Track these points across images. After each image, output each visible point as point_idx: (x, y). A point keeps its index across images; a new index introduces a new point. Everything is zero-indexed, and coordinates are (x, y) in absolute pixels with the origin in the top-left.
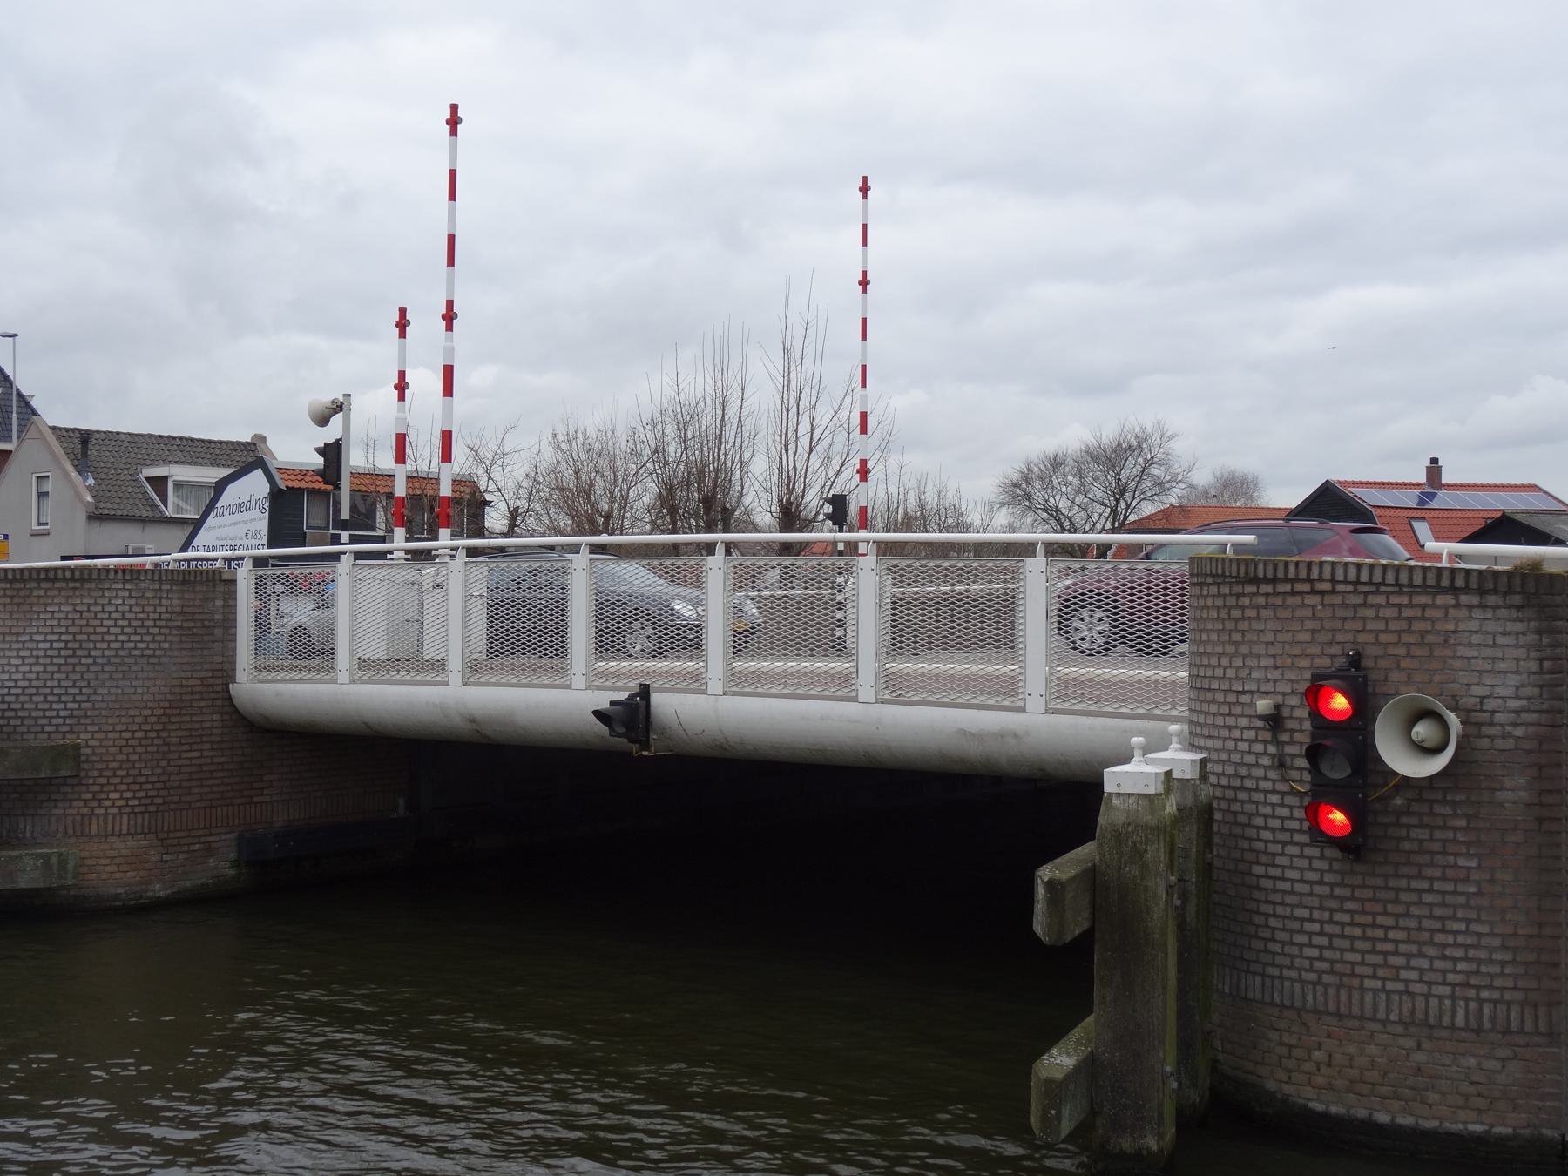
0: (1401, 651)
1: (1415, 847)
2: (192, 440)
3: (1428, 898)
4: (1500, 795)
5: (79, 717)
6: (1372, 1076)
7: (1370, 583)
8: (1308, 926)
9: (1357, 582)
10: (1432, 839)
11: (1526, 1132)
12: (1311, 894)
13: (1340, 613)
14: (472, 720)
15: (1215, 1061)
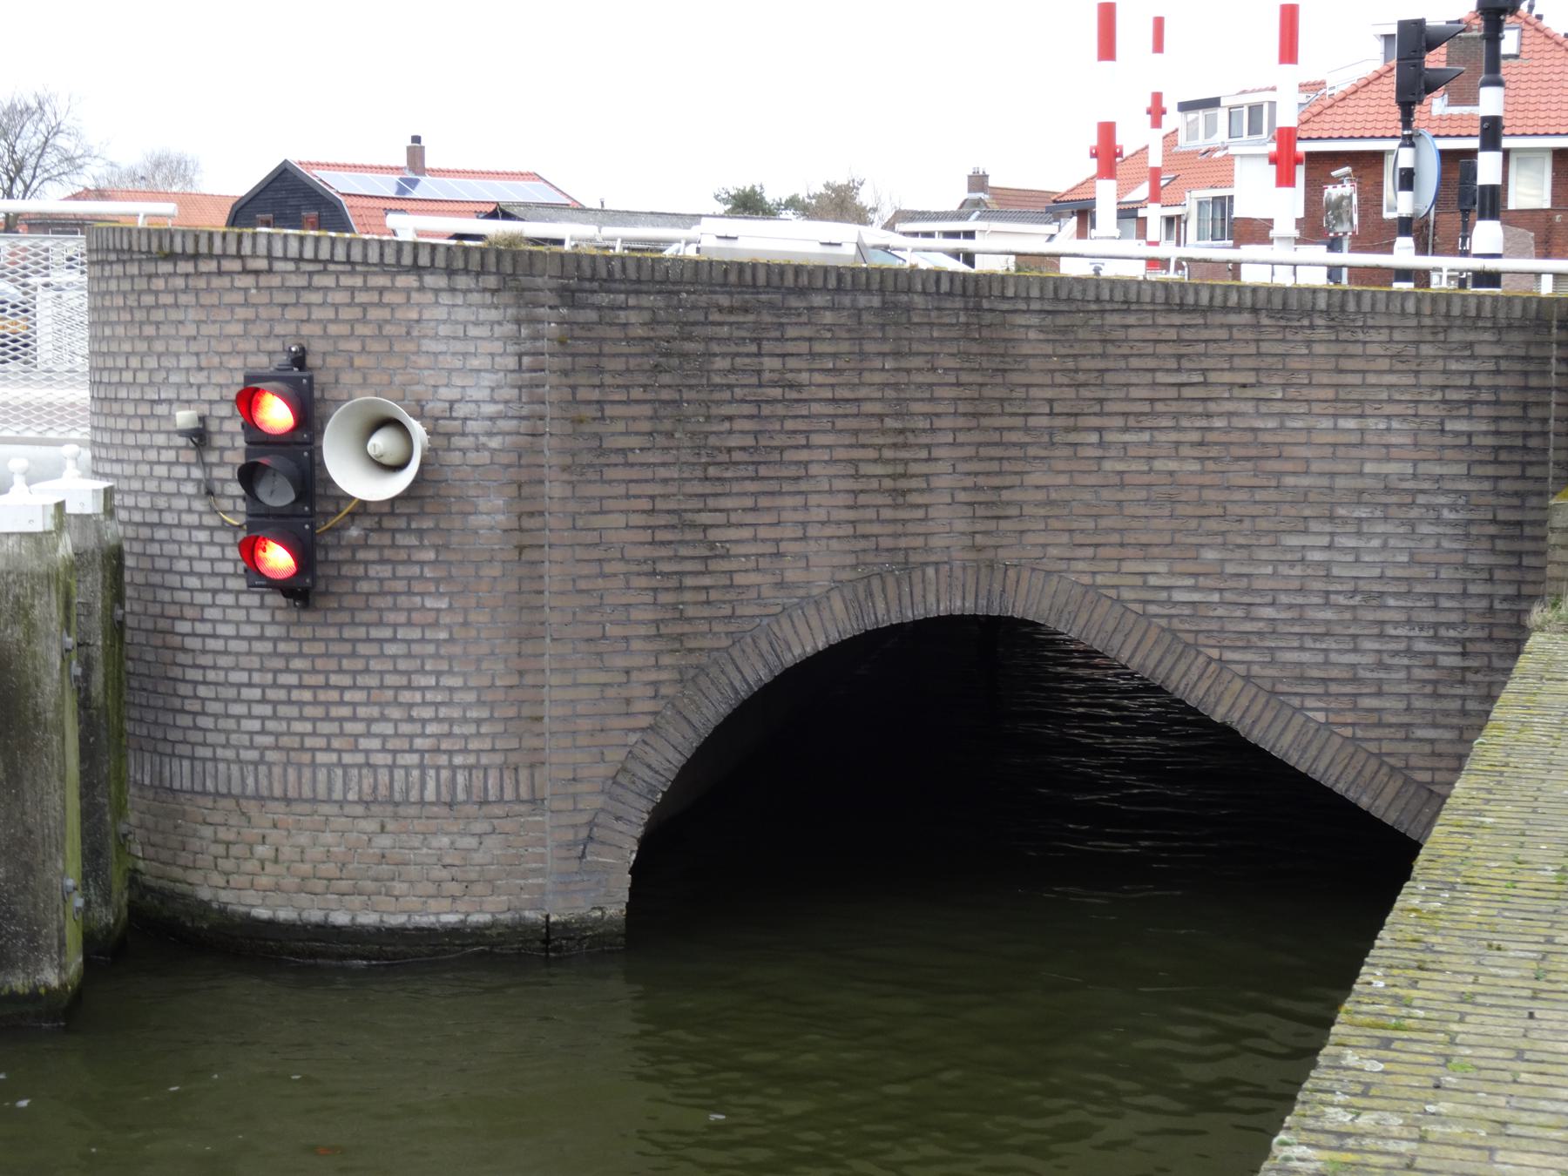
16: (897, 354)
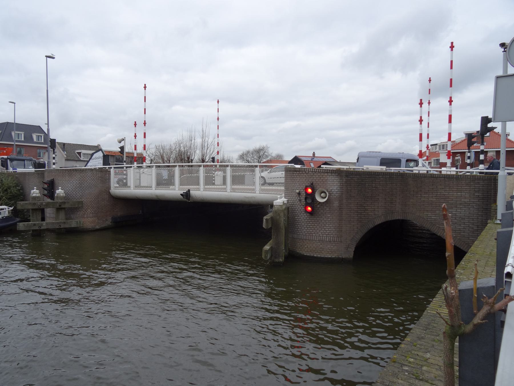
0: (319, 182)
1: (321, 213)
2: (86, 145)
3: (323, 221)
4: (334, 205)
5: (82, 196)
6: (314, 249)
7: (314, 172)
8: (304, 226)
9: (312, 171)
10: (323, 212)
11: (337, 257)
12: (305, 221)
13: (310, 176)
14: (157, 196)
15: (289, 248)
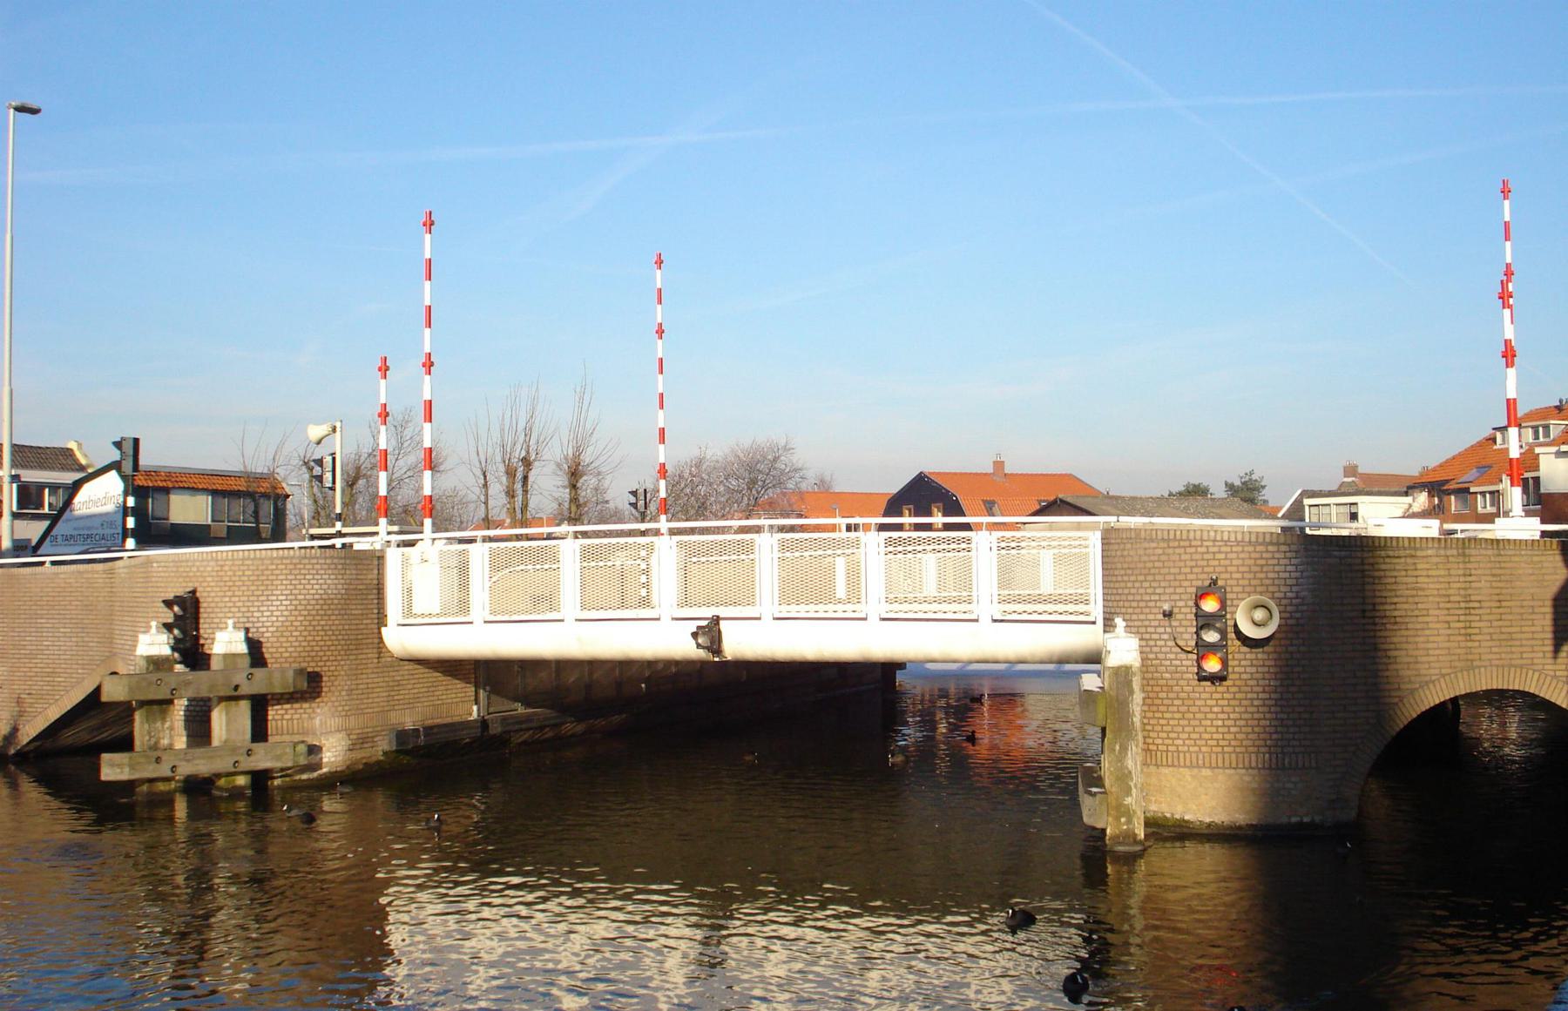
9: (1215, 541)
16: (1465, 575)
